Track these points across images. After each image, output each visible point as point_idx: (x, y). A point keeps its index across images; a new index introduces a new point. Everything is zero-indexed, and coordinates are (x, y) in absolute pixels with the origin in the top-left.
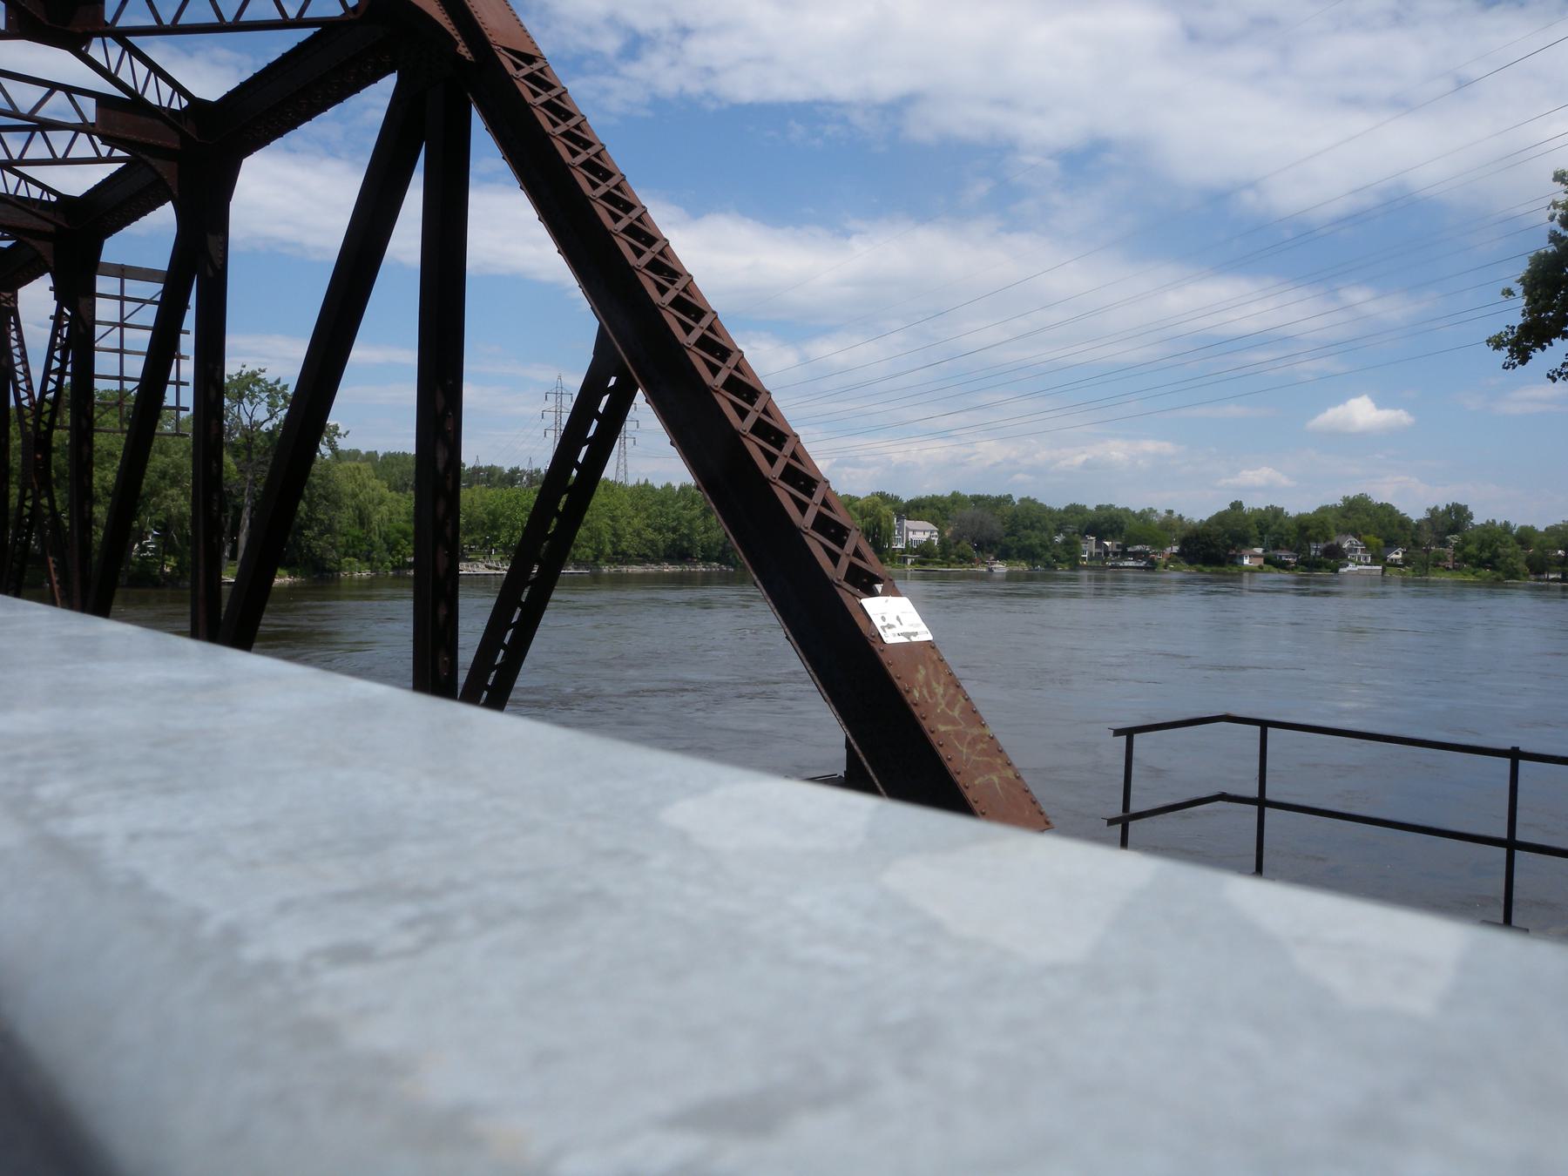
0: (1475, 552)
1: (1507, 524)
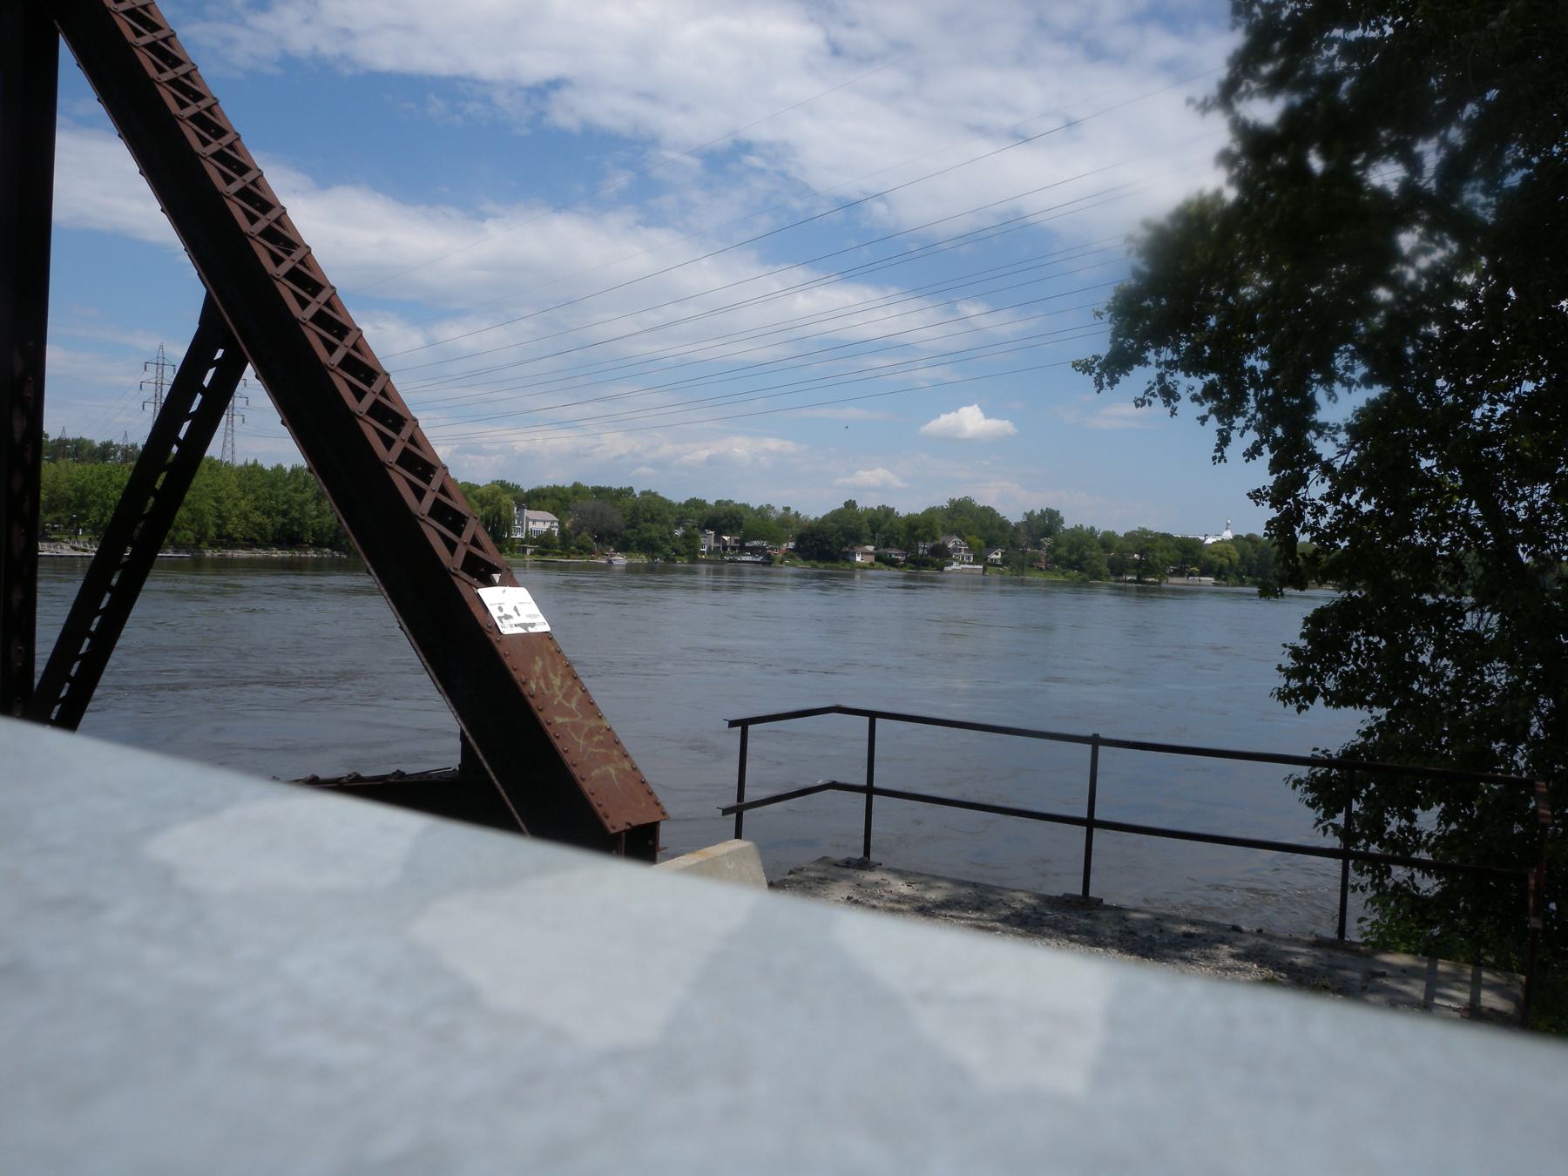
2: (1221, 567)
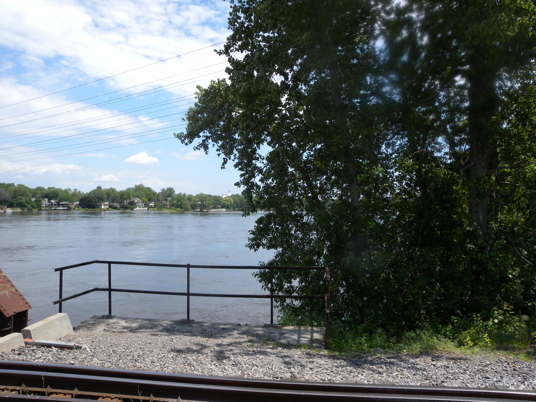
0: (176, 203)
1: (185, 194)
2: (228, 205)
